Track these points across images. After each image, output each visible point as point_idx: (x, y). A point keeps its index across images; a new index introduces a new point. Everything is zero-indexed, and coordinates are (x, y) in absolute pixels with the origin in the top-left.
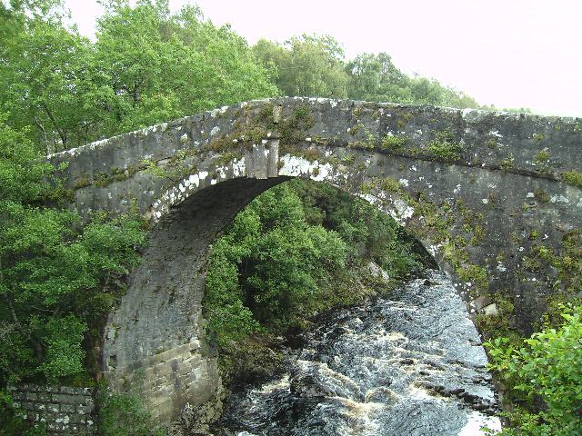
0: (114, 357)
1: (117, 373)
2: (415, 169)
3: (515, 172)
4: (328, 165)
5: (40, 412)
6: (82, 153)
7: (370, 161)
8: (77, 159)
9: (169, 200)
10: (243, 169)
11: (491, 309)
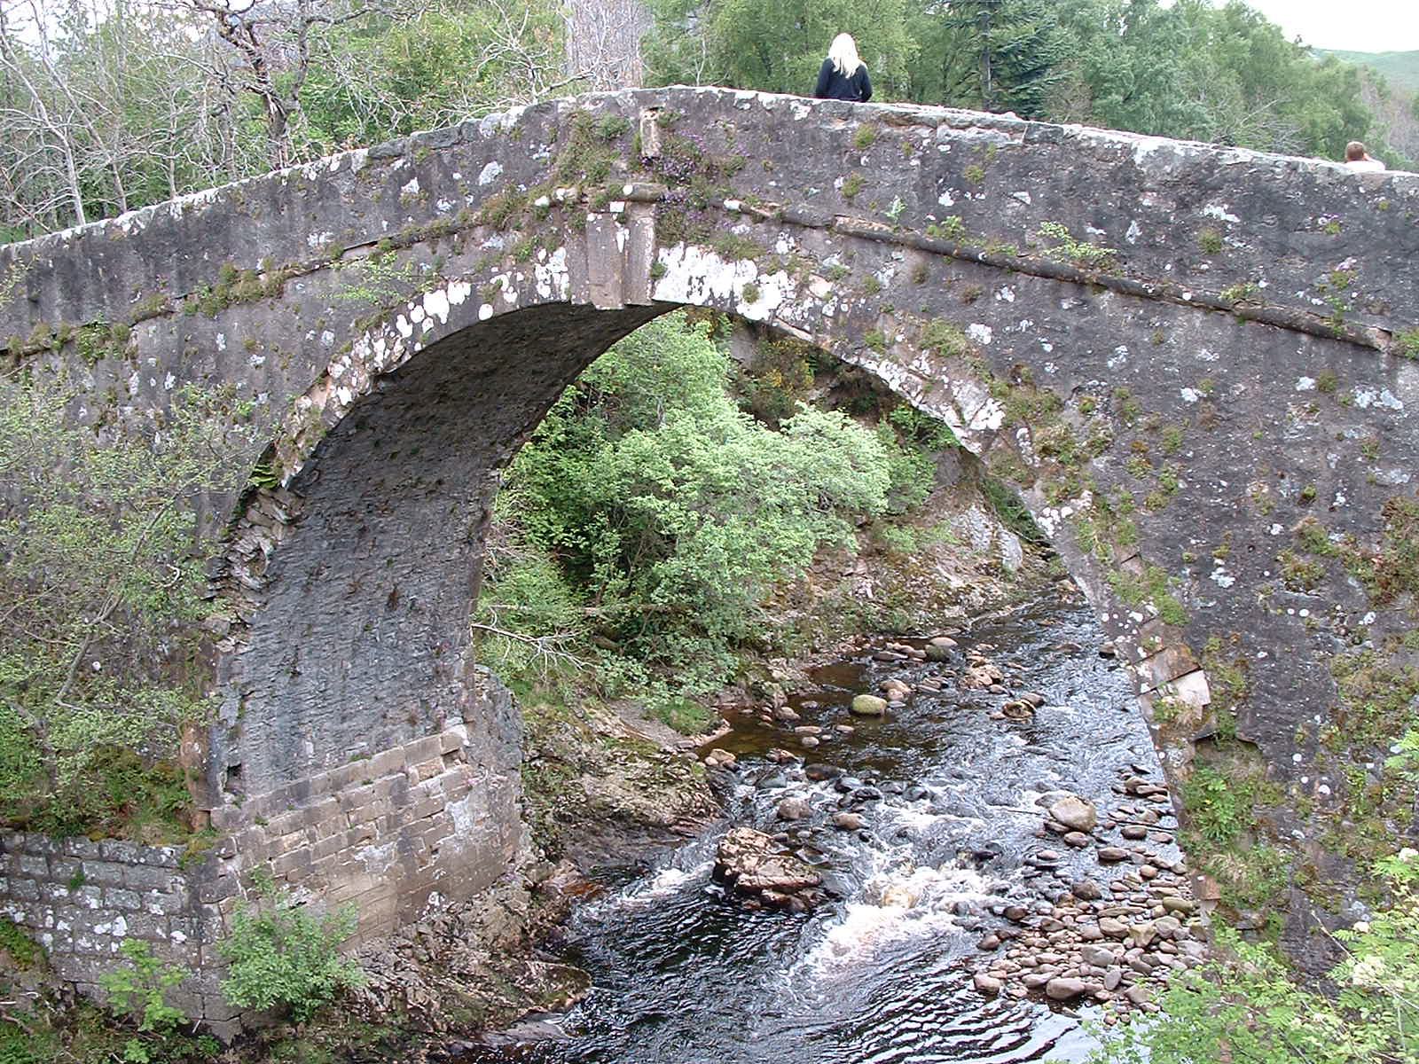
0: (235, 771)
1: (246, 811)
2: (1011, 298)
3: (1267, 321)
4: (782, 275)
5: (56, 904)
6: (152, 226)
7: (896, 269)
8: (139, 242)
9: (371, 358)
10: (563, 282)
11: (1195, 689)
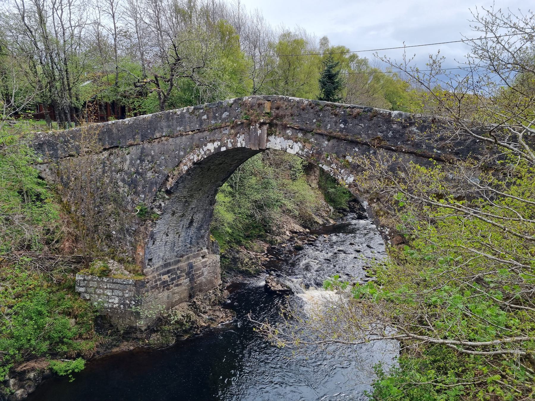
2: (357, 150)
